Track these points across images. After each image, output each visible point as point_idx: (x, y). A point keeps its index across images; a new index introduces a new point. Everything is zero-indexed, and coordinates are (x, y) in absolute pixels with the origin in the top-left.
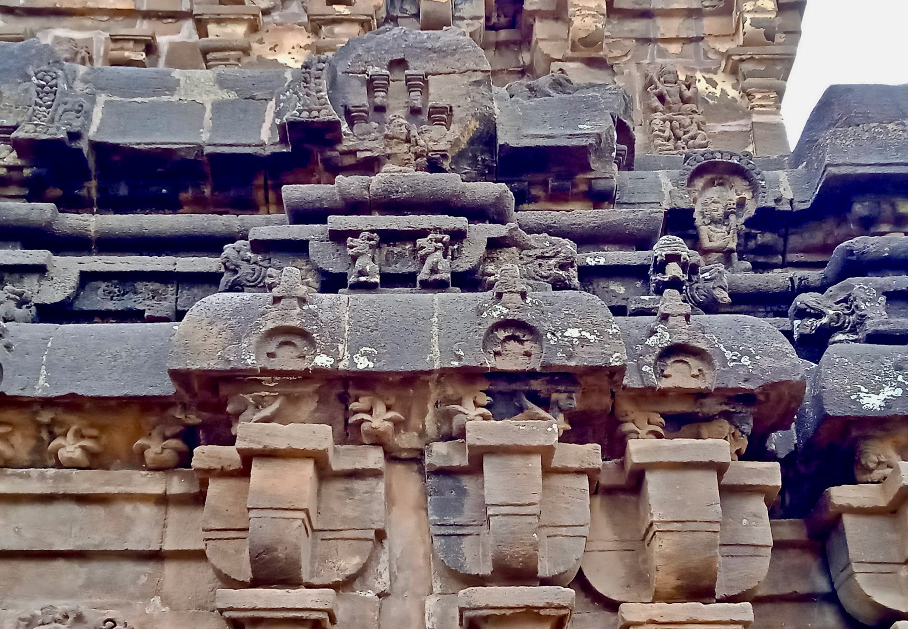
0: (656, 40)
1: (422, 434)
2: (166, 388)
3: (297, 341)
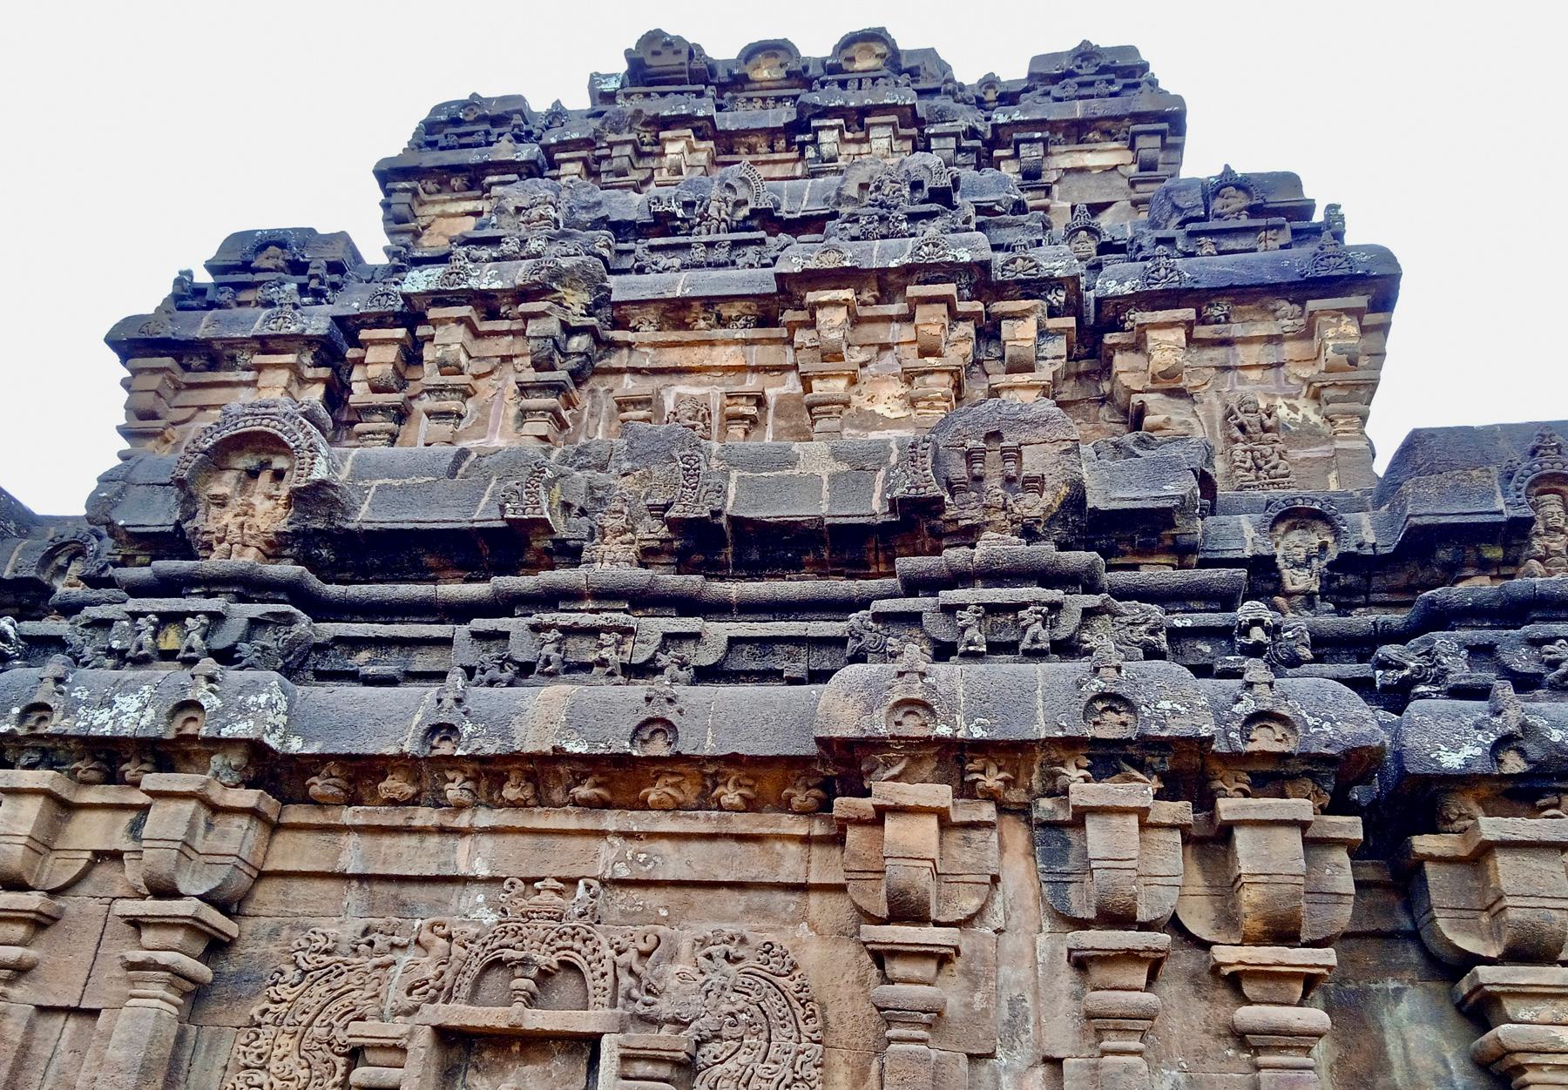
0: (1236, 368)
1: (1029, 790)
2: (812, 749)
3: (920, 711)
